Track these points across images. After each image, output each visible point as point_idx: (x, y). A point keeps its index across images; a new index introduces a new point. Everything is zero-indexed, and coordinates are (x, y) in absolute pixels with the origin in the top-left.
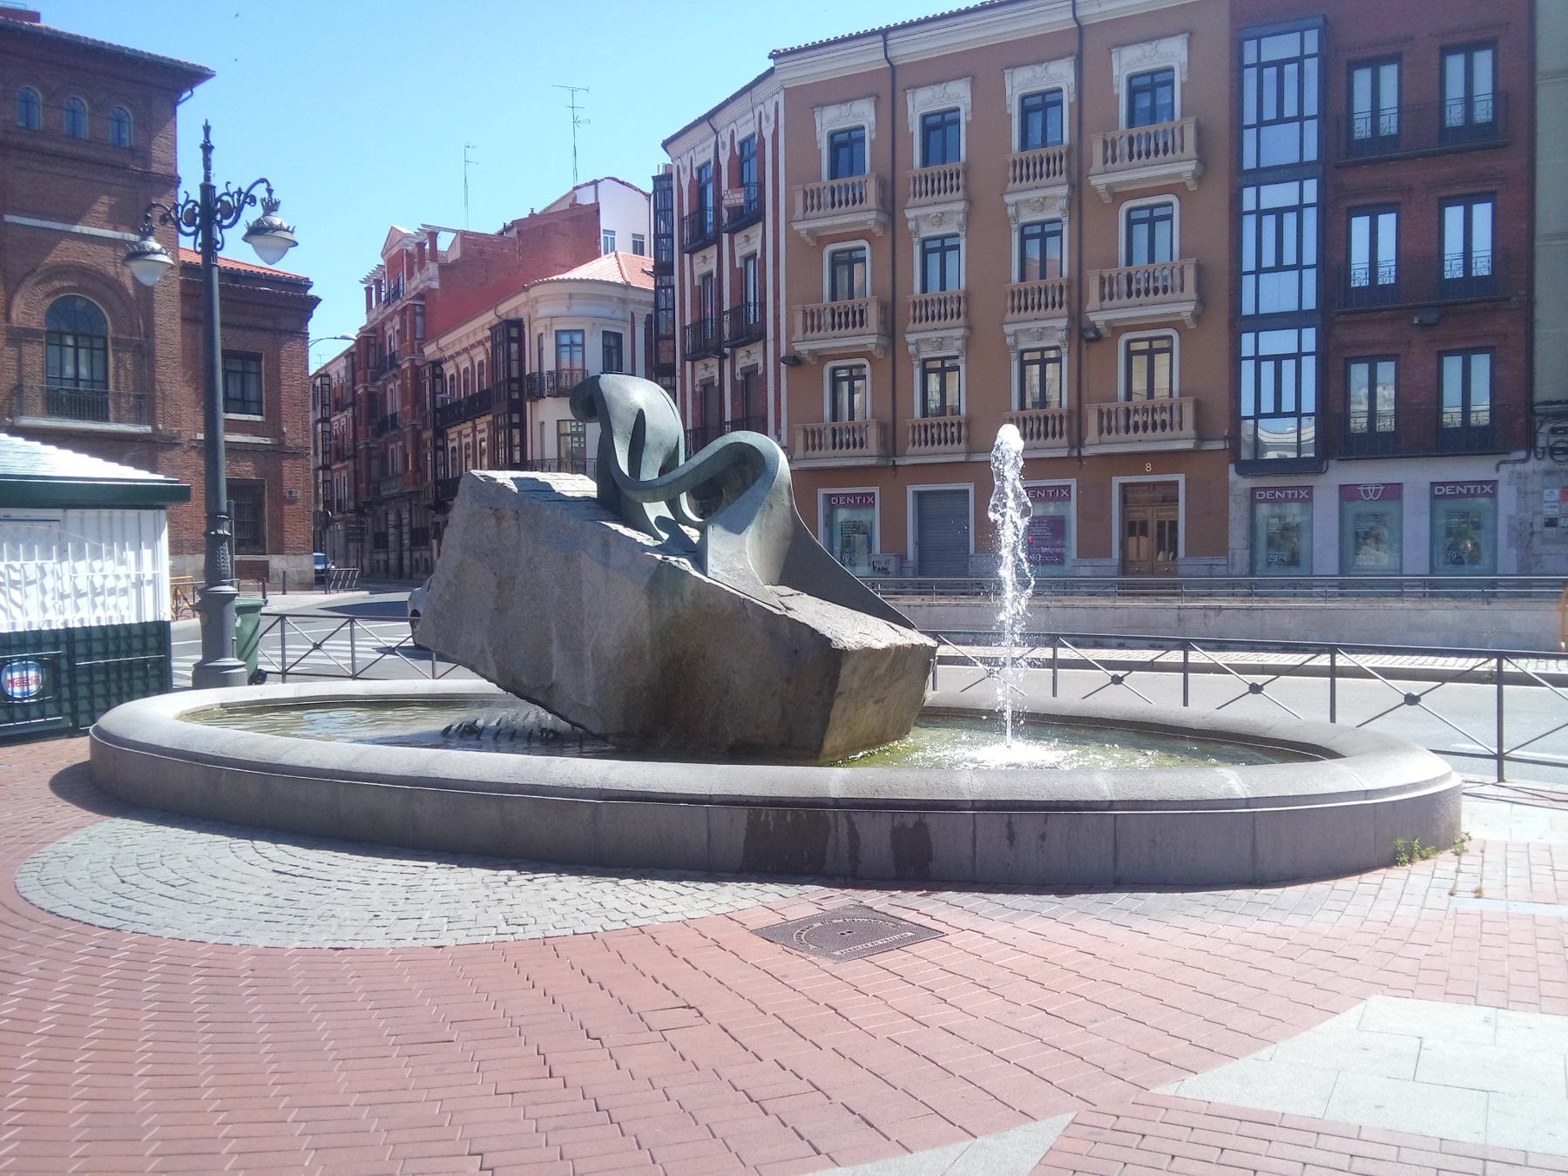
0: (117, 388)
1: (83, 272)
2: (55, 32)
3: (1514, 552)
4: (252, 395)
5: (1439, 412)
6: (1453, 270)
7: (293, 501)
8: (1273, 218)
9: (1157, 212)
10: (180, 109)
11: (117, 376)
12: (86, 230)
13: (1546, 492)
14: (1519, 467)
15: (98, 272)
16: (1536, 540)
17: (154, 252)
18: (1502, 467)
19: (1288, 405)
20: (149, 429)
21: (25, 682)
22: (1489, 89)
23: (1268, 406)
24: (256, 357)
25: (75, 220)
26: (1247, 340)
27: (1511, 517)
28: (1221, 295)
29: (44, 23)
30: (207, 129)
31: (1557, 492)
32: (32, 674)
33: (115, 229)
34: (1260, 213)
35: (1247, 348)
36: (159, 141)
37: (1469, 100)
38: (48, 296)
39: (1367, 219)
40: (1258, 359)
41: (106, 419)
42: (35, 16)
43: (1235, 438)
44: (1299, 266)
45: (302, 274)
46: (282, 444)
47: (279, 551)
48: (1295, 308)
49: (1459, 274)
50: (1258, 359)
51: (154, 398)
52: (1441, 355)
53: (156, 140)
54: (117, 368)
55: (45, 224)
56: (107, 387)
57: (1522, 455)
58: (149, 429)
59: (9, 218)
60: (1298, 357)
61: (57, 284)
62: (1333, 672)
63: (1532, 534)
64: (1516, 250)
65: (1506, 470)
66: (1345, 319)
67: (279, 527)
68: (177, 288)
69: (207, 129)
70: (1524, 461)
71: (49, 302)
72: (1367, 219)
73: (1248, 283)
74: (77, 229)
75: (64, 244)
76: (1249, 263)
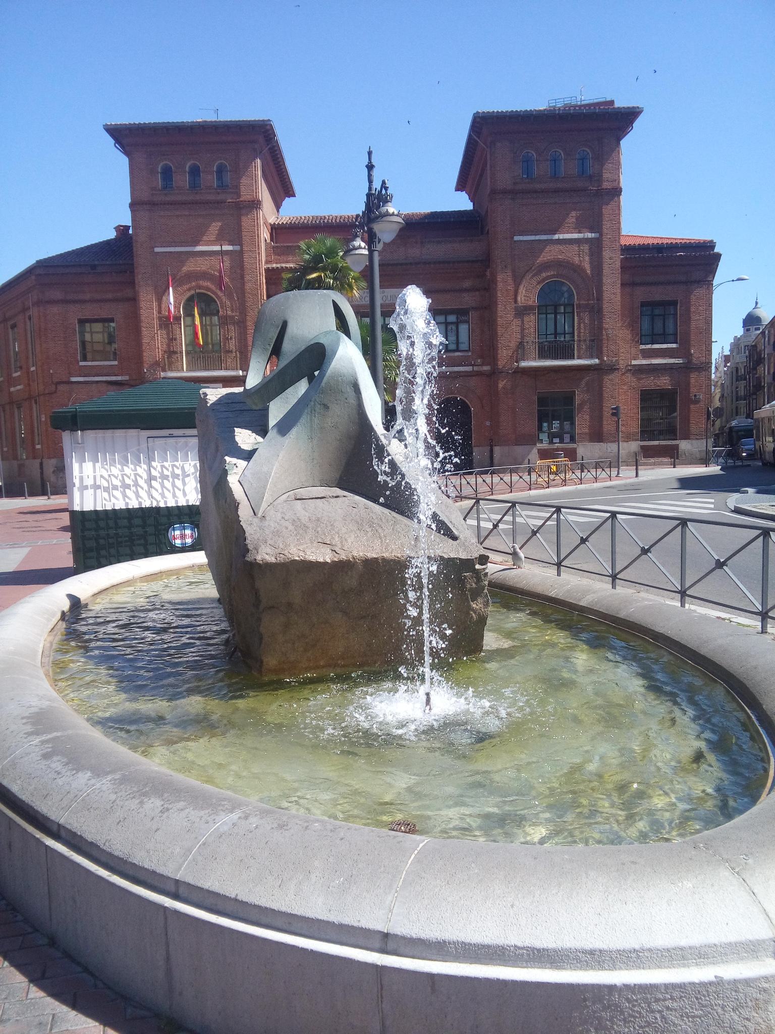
0: (579, 336)
1: (559, 264)
2: (628, 108)
4: (670, 330)
7: (697, 402)
10: (623, 143)
11: (579, 328)
12: (561, 236)
15: (568, 262)
17: (360, 247)
20: (597, 361)
21: (183, 537)
24: (674, 303)
25: (196, 243)
29: (617, 105)
30: (370, 153)
32: (188, 532)
33: (580, 232)
36: (608, 166)
38: (539, 283)
41: (572, 357)
42: (612, 102)
45: (709, 239)
46: (690, 362)
47: (686, 437)
51: (601, 340)
53: (605, 167)
54: (579, 324)
55: (538, 237)
56: (573, 337)
58: (597, 361)
59: (516, 238)
61: (544, 275)
67: (686, 420)
68: (618, 264)
69: (370, 153)
71: (539, 287)
74: (556, 237)
75: (548, 248)
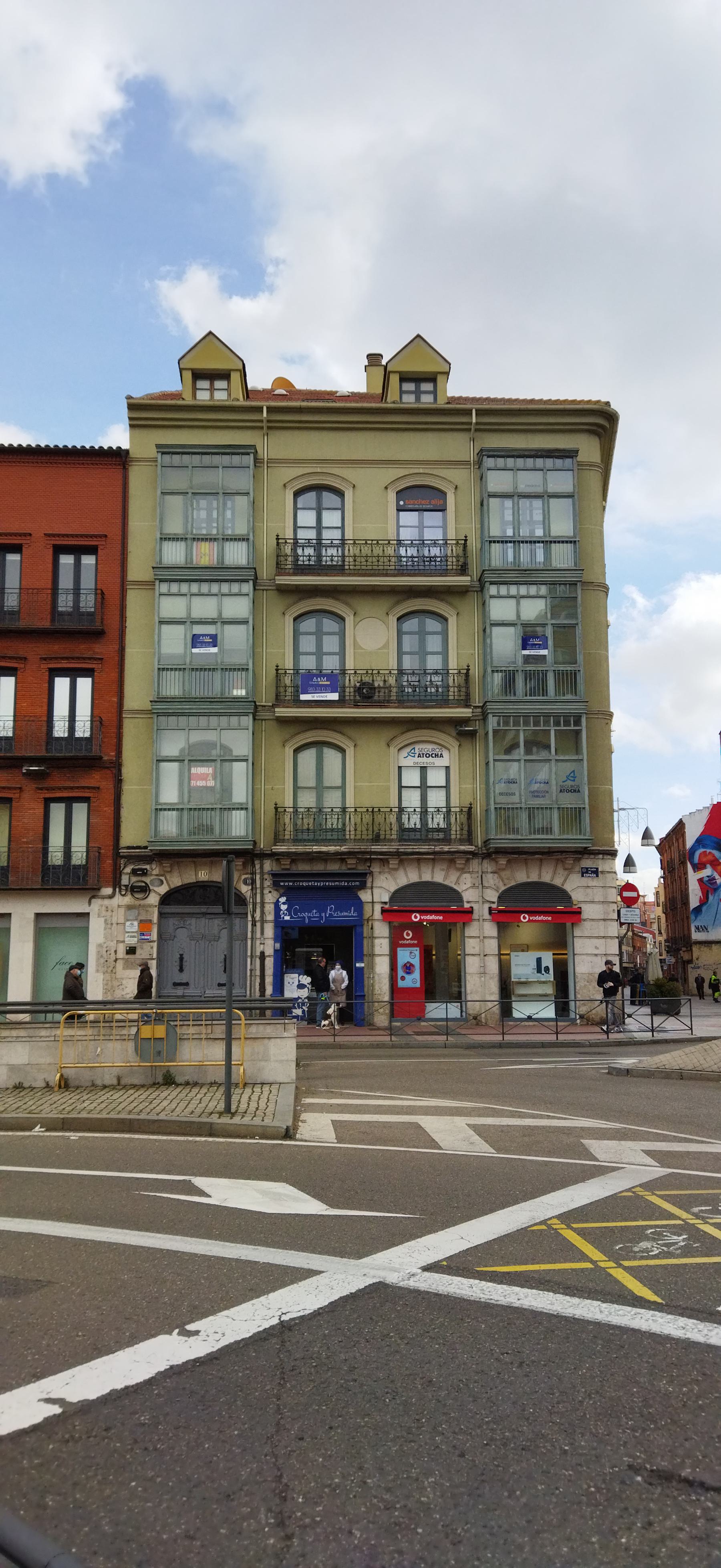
3: (101, 976)
5: (45, 851)
6: (60, 730)
13: (128, 923)
14: (107, 902)
16: (120, 965)
18: (93, 900)
27: (100, 946)
31: (136, 923)
37: (77, 590)
39: (68, 679)
42: (336, 392)
52: (48, 802)
57: (108, 891)
62: (285, 1024)
63: (116, 960)
65: (97, 904)
70: (111, 897)
72: (68, 679)
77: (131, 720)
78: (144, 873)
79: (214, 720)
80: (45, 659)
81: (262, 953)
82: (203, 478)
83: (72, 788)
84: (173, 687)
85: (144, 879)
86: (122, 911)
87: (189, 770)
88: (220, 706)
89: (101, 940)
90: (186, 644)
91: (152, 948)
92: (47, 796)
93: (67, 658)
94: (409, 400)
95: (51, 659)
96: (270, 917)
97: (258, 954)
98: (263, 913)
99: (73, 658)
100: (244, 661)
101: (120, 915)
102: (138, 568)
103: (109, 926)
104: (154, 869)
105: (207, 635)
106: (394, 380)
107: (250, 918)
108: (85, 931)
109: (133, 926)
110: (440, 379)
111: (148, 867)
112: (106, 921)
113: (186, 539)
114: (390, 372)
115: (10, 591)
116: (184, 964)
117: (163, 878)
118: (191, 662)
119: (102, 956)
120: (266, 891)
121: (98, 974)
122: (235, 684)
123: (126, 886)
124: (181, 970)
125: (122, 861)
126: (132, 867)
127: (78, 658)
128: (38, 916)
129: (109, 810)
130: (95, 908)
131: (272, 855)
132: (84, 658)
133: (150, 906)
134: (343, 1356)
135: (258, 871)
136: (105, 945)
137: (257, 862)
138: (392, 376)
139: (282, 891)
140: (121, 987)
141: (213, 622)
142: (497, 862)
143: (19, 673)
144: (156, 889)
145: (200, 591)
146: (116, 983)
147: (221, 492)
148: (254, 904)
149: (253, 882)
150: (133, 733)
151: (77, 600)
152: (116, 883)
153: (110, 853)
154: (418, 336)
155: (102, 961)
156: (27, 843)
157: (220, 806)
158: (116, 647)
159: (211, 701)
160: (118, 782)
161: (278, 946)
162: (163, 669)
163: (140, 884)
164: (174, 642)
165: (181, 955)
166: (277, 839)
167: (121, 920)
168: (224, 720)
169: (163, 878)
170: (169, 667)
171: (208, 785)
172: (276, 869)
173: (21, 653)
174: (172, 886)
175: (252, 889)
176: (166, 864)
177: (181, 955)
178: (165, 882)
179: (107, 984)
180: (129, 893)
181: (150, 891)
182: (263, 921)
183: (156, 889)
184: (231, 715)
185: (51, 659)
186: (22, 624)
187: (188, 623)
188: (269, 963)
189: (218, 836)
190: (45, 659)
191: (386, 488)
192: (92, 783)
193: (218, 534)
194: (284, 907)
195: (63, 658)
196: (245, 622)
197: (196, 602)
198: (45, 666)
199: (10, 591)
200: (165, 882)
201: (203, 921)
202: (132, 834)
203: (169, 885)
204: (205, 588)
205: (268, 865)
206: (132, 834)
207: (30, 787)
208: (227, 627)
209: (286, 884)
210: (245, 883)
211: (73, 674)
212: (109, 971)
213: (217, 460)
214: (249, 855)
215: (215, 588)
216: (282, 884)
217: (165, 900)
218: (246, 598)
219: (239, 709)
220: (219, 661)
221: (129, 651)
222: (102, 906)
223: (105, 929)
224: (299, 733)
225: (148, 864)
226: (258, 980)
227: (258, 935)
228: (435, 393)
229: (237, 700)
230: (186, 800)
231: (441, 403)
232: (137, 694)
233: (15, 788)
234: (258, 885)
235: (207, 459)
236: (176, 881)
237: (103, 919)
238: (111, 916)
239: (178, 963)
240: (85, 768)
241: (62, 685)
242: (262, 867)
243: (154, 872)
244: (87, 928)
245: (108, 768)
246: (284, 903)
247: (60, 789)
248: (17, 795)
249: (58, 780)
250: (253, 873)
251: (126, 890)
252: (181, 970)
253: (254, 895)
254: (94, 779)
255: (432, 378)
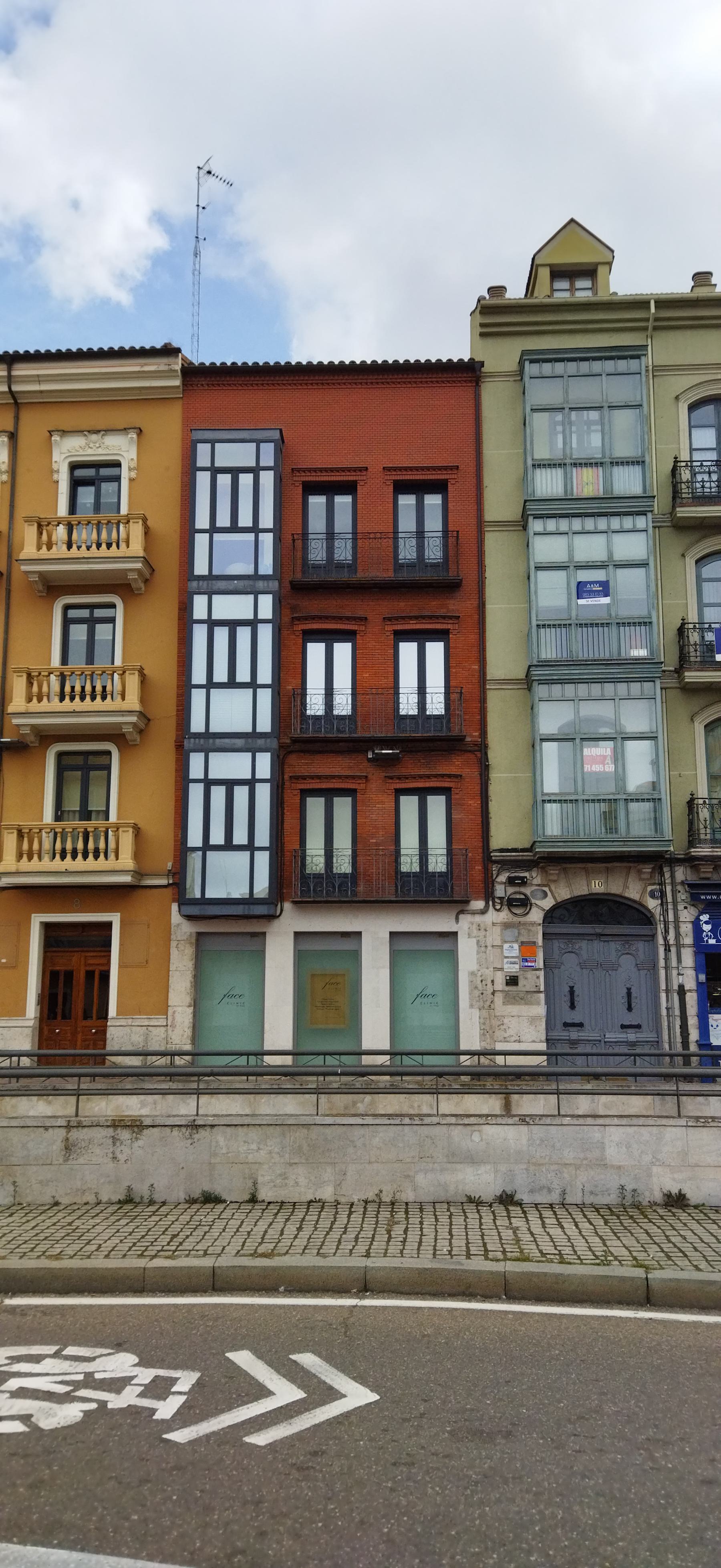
3: (476, 1013)
5: (397, 854)
6: (408, 705)
8: (228, 477)
9: (98, 613)
13: (506, 946)
14: (478, 918)
18: (461, 916)
19: (240, 837)
22: (439, 526)
23: (217, 837)
26: (196, 762)
27: (472, 974)
28: (167, 707)
31: (516, 946)
34: (212, 624)
35: (196, 769)
39: (323, 645)
40: (208, 783)
43: (179, 875)
44: (253, 685)
48: (250, 730)
49: (414, 711)
50: (215, 471)
57: (479, 904)
60: (255, 471)
64: (469, 685)
65: (465, 919)
66: (303, 750)
70: (483, 912)
72: (323, 645)
73: (198, 698)
76: (199, 676)
77: (495, 692)
78: (524, 882)
79: (609, 688)
80: (390, 619)
81: (681, 987)
82: (584, 391)
83: (429, 777)
84: (550, 647)
85: (523, 890)
86: (497, 930)
87: (582, 751)
88: (615, 671)
89: (474, 967)
90: (569, 594)
91: (538, 977)
92: (399, 786)
93: (416, 618)
94: (561, 296)
95: (396, 618)
96: (688, 940)
97: (676, 987)
98: (678, 935)
99: (423, 617)
100: (644, 613)
101: (494, 936)
102: (499, 504)
103: (483, 949)
104: (535, 877)
105: (596, 582)
106: (544, 274)
107: (661, 941)
108: (452, 955)
109: (513, 950)
110: (601, 270)
111: (526, 874)
112: (478, 942)
113: (565, 464)
114: (538, 266)
115: (430, 534)
116: (633, 1000)
117: (546, 889)
118: (577, 615)
119: (476, 988)
120: (680, 907)
121: (473, 1010)
122: (633, 643)
123: (501, 898)
124: (573, 1006)
125: (495, 868)
126: (507, 874)
127: (431, 617)
128: (392, 934)
129: (475, 804)
130: (464, 926)
131: (690, 861)
132: (437, 617)
133: (533, 924)
134: (357, 1505)
135: (668, 881)
136: (480, 974)
137: (666, 869)
138: (540, 270)
139: (701, 906)
140: (502, 1027)
141: (602, 566)
142: (546, 872)
143: (358, 637)
144: (539, 902)
145: (545, 529)
146: (495, 1023)
147: (606, 405)
148: (666, 923)
149: (663, 895)
150: (500, 707)
151: (420, 548)
152: (488, 895)
153: (479, 857)
154: (572, 221)
155: (477, 993)
156: (377, 844)
157: (625, 797)
158: (475, 603)
159: (607, 663)
160: (484, 768)
161: (702, 978)
162: (544, 626)
163: (518, 896)
164: (552, 592)
165: (572, 988)
166: (693, 839)
167: (498, 942)
168: (622, 688)
169: (546, 889)
170: (551, 623)
171: (607, 770)
172: (692, 878)
173: (360, 613)
174: (559, 900)
175: (662, 904)
176: (553, 871)
177: (572, 988)
178: (549, 894)
179: (484, 1024)
180: (505, 908)
181: (531, 905)
182: (679, 946)
183: (539, 902)
184: (628, 681)
185: (396, 618)
186: (361, 575)
187: (572, 568)
188: (692, 1000)
189: (624, 835)
190: (390, 619)
191: (677, 398)
192: (453, 770)
193: (604, 457)
194: (707, 928)
195: (411, 618)
196: (644, 565)
197: (580, 542)
198: (390, 628)
199: (430, 534)
200: (549, 894)
201: (597, 945)
202: (505, 834)
203: (554, 898)
204: (589, 524)
205: (681, 873)
206: (505, 834)
207: (376, 775)
208: (620, 572)
209: (709, 897)
210: (652, 895)
211: (421, 637)
212: (486, 1006)
213: (597, 366)
214: (652, 861)
215: (602, 523)
216: (703, 897)
217: (550, 916)
218: (644, 534)
219: (643, 672)
220: (613, 614)
221: (489, 607)
222: (472, 924)
223: (478, 953)
224: (711, 704)
225: (527, 871)
226: (678, 1023)
227: (674, 963)
228: (594, 289)
229: (637, 661)
230: (580, 789)
231: (602, 296)
232: (503, 659)
233: (360, 777)
234: (670, 899)
235: (584, 367)
236: (564, 892)
237: (474, 940)
238: (485, 937)
239: (568, 998)
240: (442, 753)
241: (408, 651)
242: (673, 876)
243: (535, 882)
244: (263, 952)
245: (470, 751)
246: (706, 923)
247: (414, 777)
248: (363, 786)
249: (412, 767)
250: (662, 884)
251: (502, 904)
252: (573, 1006)
253: (665, 912)
254: (455, 765)
255: (590, 272)
